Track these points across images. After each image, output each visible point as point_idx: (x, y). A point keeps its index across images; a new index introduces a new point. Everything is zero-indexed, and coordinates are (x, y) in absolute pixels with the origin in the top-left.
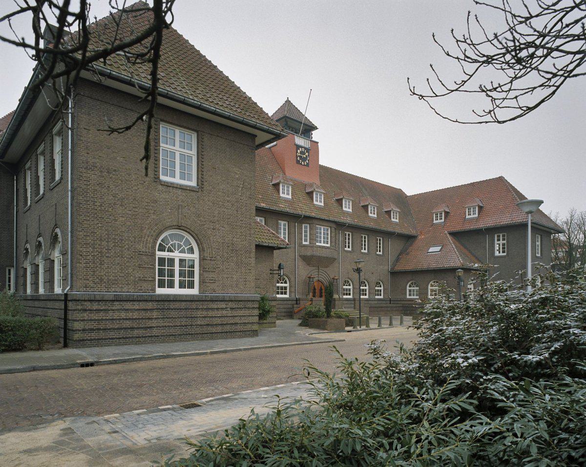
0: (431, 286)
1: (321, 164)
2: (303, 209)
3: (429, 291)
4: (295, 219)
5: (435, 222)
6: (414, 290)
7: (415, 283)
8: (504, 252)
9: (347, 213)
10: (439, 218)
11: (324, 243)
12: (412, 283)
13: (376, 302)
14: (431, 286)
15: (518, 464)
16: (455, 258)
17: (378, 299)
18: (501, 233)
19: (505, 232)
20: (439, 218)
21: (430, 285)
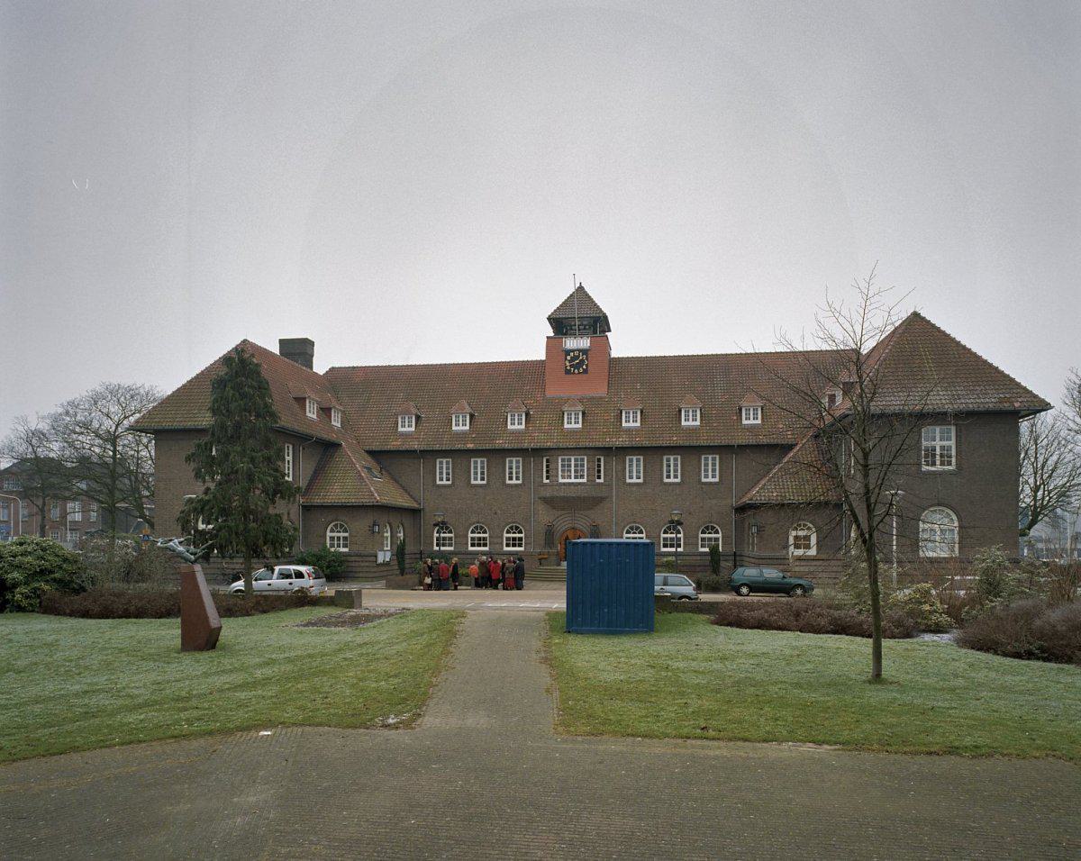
0: (331, 532)
1: (324, 372)
2: (540, 440)
3: (328, 538)
4: (532, 454)
5: (400, 429)
6: (339, 538)
7: (342, 526)
8: (482, 479)
9: (464, 433)
10: (407, 423)
11: (576, 477)
12: (336, 526)
13: (699, 558)
14: (331, 532)
15: (514, 860)
16: (380, 489)
17: (702, 552)
18: (710, 454)
19: (716, 454)
20: (407, 423)
21: (328, 531)
